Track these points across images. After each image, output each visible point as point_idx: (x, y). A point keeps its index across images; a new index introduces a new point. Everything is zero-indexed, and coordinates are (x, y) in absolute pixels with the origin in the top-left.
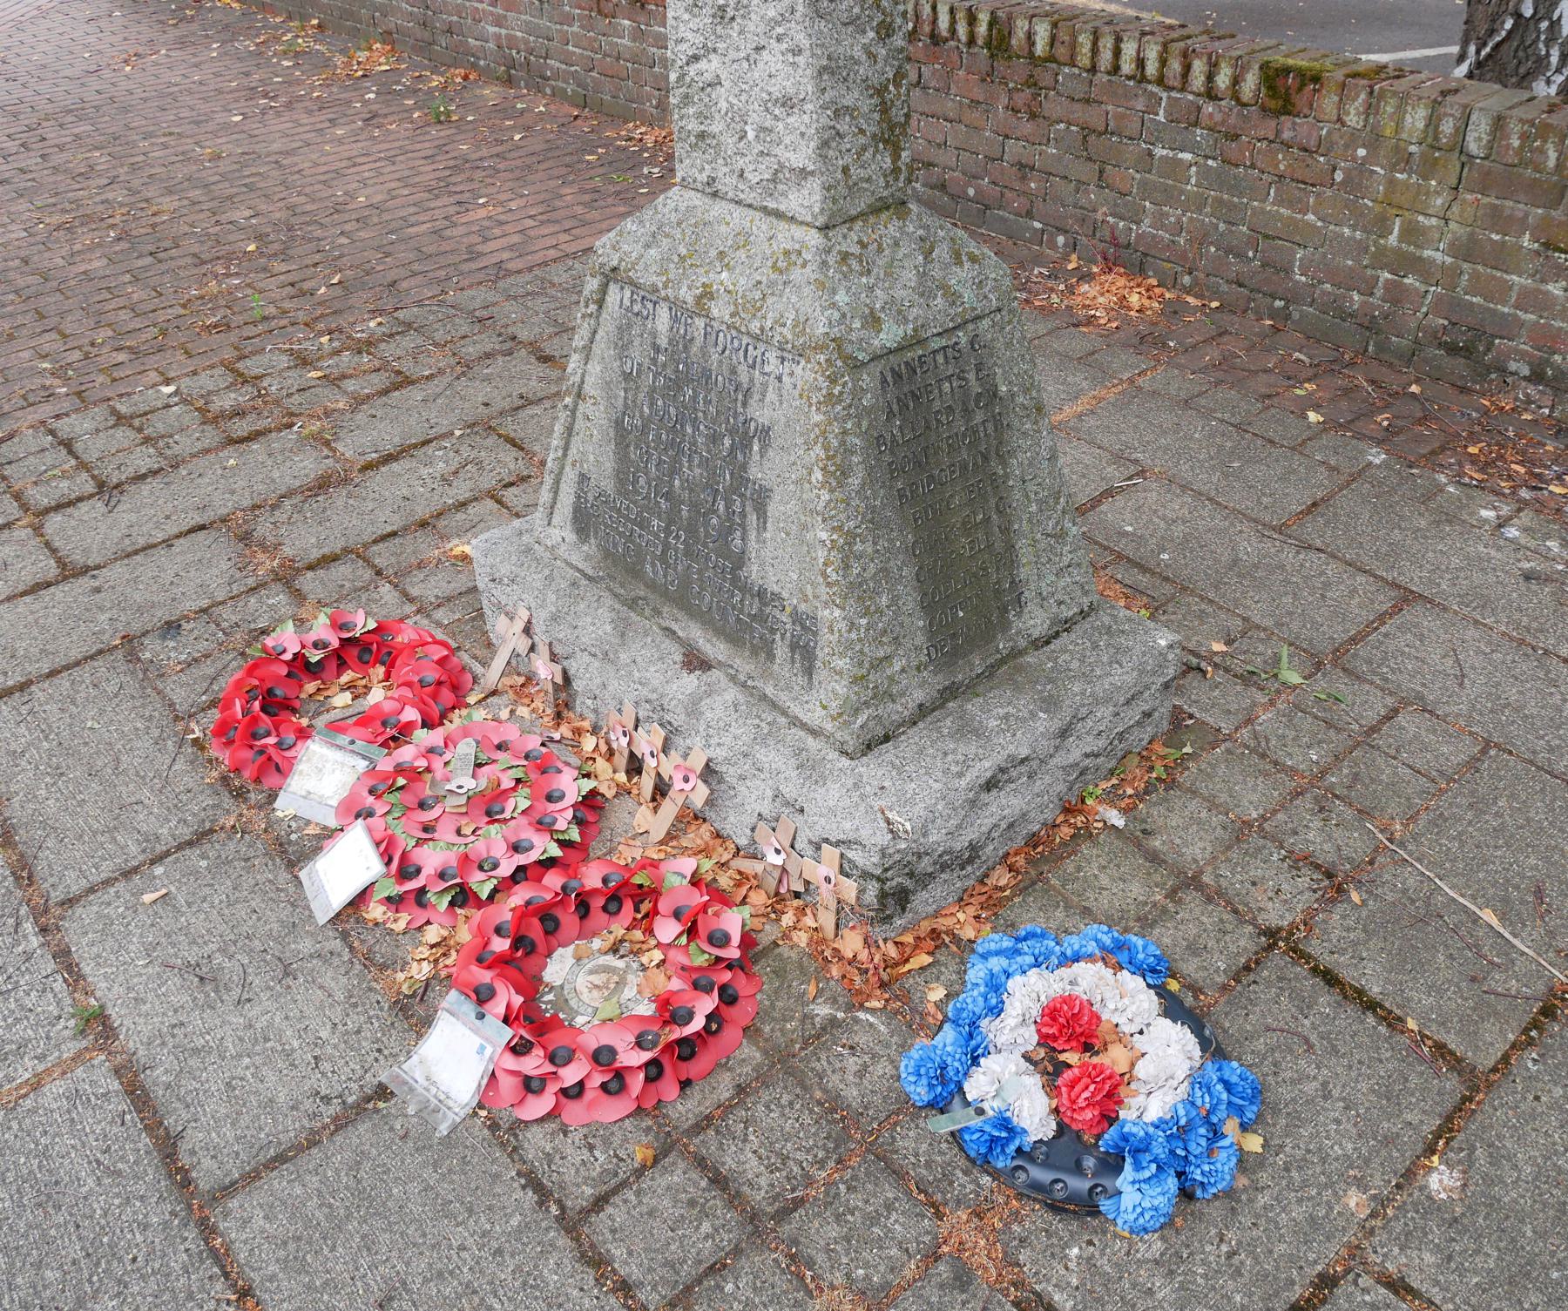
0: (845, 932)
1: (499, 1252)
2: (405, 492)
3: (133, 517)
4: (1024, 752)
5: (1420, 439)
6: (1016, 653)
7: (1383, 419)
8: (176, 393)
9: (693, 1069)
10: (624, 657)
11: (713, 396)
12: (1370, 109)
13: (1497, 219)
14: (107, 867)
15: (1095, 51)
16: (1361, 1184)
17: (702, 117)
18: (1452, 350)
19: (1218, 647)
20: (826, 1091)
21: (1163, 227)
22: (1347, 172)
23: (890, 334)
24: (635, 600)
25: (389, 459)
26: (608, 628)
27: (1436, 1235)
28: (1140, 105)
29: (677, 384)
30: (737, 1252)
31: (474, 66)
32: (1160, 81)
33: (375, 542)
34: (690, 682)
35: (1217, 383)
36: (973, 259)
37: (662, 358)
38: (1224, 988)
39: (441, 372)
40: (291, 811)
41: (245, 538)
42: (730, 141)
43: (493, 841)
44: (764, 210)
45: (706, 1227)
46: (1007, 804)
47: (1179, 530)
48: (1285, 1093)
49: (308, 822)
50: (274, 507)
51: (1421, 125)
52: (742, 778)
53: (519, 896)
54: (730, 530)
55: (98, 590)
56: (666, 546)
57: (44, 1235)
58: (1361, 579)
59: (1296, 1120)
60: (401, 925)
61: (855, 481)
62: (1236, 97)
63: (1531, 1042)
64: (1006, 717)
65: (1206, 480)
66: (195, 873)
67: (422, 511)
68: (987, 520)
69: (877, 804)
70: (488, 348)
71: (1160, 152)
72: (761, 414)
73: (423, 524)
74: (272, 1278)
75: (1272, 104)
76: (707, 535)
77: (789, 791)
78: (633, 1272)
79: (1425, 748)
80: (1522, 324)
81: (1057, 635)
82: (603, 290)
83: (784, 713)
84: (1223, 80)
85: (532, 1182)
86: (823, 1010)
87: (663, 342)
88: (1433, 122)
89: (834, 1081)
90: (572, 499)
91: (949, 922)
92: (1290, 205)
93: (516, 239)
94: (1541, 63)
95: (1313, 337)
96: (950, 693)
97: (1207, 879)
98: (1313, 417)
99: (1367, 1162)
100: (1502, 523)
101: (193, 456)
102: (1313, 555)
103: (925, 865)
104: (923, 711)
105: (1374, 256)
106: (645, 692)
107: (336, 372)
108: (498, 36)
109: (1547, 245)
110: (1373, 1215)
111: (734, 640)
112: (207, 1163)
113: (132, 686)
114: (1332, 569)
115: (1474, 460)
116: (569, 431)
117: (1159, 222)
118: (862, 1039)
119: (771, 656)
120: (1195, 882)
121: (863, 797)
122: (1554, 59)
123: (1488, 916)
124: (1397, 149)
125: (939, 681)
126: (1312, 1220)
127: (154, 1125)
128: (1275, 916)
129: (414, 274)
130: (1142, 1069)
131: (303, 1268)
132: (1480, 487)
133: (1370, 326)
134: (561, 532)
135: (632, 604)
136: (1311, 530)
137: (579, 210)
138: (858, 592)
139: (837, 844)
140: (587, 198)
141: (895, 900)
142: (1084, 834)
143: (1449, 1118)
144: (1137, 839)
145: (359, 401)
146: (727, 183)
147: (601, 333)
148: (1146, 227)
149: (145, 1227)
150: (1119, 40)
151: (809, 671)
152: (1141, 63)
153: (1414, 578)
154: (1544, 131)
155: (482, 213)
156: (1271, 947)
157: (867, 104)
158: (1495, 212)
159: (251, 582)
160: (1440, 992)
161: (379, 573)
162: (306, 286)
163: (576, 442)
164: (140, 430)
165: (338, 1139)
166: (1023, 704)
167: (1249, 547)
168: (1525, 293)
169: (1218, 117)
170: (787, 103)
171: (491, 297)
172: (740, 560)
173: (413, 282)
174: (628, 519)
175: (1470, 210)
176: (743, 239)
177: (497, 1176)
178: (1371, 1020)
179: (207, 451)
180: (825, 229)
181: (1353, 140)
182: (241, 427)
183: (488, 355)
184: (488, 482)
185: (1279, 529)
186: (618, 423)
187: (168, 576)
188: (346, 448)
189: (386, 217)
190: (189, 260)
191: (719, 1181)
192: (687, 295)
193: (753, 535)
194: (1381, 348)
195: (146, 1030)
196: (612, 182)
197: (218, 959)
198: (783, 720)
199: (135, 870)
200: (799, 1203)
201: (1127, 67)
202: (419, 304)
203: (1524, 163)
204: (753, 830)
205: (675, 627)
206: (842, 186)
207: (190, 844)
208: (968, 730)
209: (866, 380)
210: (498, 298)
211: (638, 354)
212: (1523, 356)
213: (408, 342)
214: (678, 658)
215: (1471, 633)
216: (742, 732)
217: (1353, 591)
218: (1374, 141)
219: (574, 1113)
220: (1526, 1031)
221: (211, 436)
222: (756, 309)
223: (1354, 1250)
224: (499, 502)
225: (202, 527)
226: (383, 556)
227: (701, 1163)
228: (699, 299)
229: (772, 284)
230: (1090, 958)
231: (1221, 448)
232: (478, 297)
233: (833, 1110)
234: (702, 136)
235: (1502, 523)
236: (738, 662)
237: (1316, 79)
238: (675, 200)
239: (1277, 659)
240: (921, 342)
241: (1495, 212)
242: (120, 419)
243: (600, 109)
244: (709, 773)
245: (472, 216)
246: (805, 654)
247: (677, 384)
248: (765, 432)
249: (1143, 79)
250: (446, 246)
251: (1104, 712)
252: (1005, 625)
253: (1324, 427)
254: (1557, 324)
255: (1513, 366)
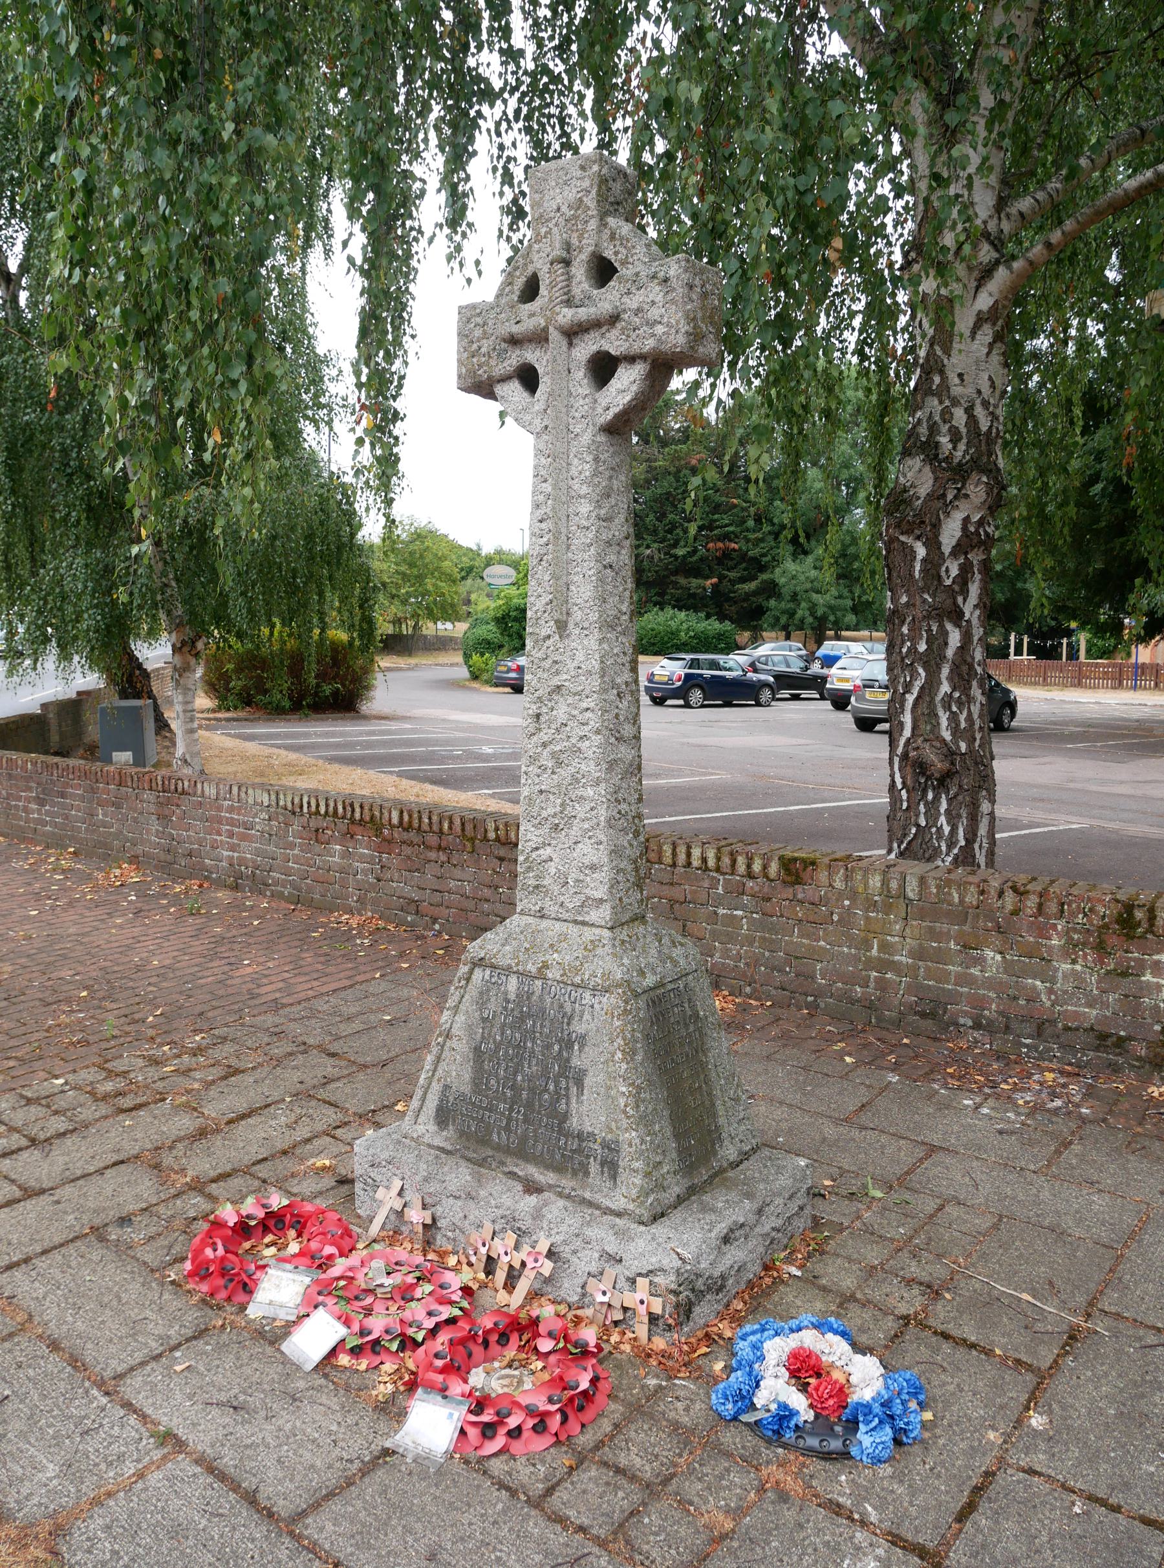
0: (654, 1339)
1: (495, 1523)
2: (263, 1135)
3: (67, 1159)
4: (742, 1220)
5: (915, 1067)
6: (722, 1171)
7: (892, 1058)
8: (66, 1083)
9: (587, 1416)
10: (483, 1193)
11: (547, 1023)
12: (847, 878)
13: (933, 935)
14: (139, 1356)
15: (674, 854)
16: (993, 1428)
17: (537, 877)
18: (923, 1015)
19: (827, 1183)
20: (668, 1420)
21: (728, 957)
22: (839, 914)
23: (650, 980)
24: (484, 1159)
25: (243, 1117)
26: (468, 1178)
27: (1042, 1446)
28: (706, 884)
29: (522, 1019)
30: (644, 1504)
31: (206, 878)
32: (718, 869)
33: (253, 1164)
34: (533, 1200)
35: (785, 1046)
36: (682, 945)
37: (511, 1006)
38: (886, 1347)
39: (261, 1065)
40: (261, 1314)
41: (157, 1167)
42: (556, 889)
43: (416, 1311)
44: (576, 922)
45: (620, 1494)
46: (735, 1255)
47: (784, 1125)
48: (938, 1392)
49: (274, 1320)
50: (171, 1148)
51: (879, 885)
52: (575, 1252)
53: (443, 1337)
54: (558, 1100)
55: (58, 1202)
56: (509, 1119)
57: (182, 1553)
58: (902, 1142)
59: (947, 1405)
60: (363, 1367)
61: (639, 1058)
62: (766, 876)
63: (1067, 1353)
64: (727, 1201)
65: (795, 1098)
66: (205, 1353)
67: (280, 1145)
68: (700, 1087)
69: (669, 1246)
70: (289, 1050)
71: (721, 911)
72: (579, 1028)
73: (285, 1152)
74: (352, 1554)
75: (789, 879)
76: (541, 1105)
77: (611, 1249)
78: (585, 1521)
79: (966, 1222)
80: (961, 994)
81: (741, 1162)
82: (471, 972)
83: (598, 1207)
84: (757, 867)
85: (502, 1486)
86: (652, 1382)
87: (512, 997)
88: (885, 883)
89: (672, 1415)
90: (436, 1103)
91: (715, 1329)
92: (808, 937)
93: (281, 985)
94: (937, 851)
95: (835, 1018)
96: (692, 1191)
97: (859, 1296)
98: (848, 1059)
99: (994, 1418)
100: (977, 1107)
101: (97, 1120)
102: (870, 1132)
103: (700, 1284)
104: (680, 1201)
105: (865, 963)
106: (500, 1212)
107: (183, 1068)
108: (231, 858)
109: (964, 946)
110: (1005, 1442)
111: (559, 1169)
112: (281, 1502)
113: (110, 1256)
114: (884, 1139)
115: (952, 1076)
116: (438, 1059)
117: (726, 954)
118: (682, 1393)
119: (587, 1173)
120: (852, 1298)
121: (659, 1244)
122: (944, 848)
123: (1025, 1296)
124: (867, 899)
125: (686, 1183)
126: (972, 1447)
127: (235, 1487)
128: (903, 1309)
129: (215, 1008)
130: (853, 1379)
131: (370, 1547)
132: (959, 1088)
133: (870, 1007)
134: (425, 1127)
135: (482, 1163)
136: (865, 1118)
137: (320, 967)
138: (644, 1121)
139: (647, 1275)
140: (322, 959)
141: (685, 1311)
142: (779, 1281)
143: (1033, 1393)
144: (812, 1280)
145: (208, 1085)
146: (552, 909)
147: (467, 997)
148: (717, 958)
149: (253, 1540)
150: (689, 847)
151: (614, 1177)
152: (704, 860)
153: (935, 1139)
154: (949, 883)
155: (249, 970)
156: (907, 1325)
157: (630, 867)
158: (931, 930)
159: (172, 1191)
160: (1010, 1335)
161: (264, 1181)
162: (136, 1016)
163: (443, 1066)
164: (48, 1106)
165: (366, 1480)
166: (733, 1196)
167: (830, 1131)
168: (958, 976)
169: (757, 889)
170: (593, 867)
171: (277, 1020)
172: (565, 1116)
173: (216, 1012)
174: (481, 1107)
175: (916, 931)
176: (563, 937)
177: (478, 1486)
178: (974, 1353)
179: (106, 1117)
180: (611, 928)
181: (841, 896)
182: (127, 1102)
183: (291, 1054)
184: (320, 1127)
185: (846, 1120)
186: (477, 1050)
187: (109, 1191)
188: (210, 1110)
189: (178, 973)
190: (37, 1003)
191: (619, 1471)
192: (532, 968)
193: (574, 1100)
194: (878, 1019)
195: (207, 1439)
196: (336, 949)
197: (242, 1398)
198: (597, 1212)
199: (160, 1355)
200: (673, 1475)
201: (696, 863)
202: (226, 1025)
203: (940, 901)
204: (583, 1287)
205: (516, 1170)
206: (619, 906)
207: (195, 1338)
208: (705, 1209)
209: (641, 1004)
210: (282, 1020)
211: (493, 1005)
212: (966, 1014)
213: (229, 1048)
214: (520, 1188)
215: (975, 1164)
216: (572, 1222)
217: (900, 1149)
218: (853, 895)
219: (517, 1447)
220: (1063, 1348)
221: (104, 1109)
222: (577, 971)
223: (1001, 1460)
224: (333, 1137)
225: (122, 1162)
226: (263, 1171)
227: (605, 1464)
228: (539, 970)
229: (585, 957)
230: (807, 1327)
231: (797, 1081)
232: (270, 1020)
233: (676, 1430)
234: (537, 887)
235: (977, 1107)
236: (564, 1182)
237: (813, 863)
238: (515, 922)
239: (865, 1186)
240: (663, 985)
241: (931, 930)
242: (29, 1101)
243: (310, 904)
244: (551, 1254)
245: (242, 972)
246: (611, 1167)
247: (522, 1019)
248: (582, 1039)
249: (707, 869)
250: (230, 991)
251: (779, 1201)
252: (715, 1153)
253: (856, 1065)
254: (981, 992)
255: (962, 1021)
